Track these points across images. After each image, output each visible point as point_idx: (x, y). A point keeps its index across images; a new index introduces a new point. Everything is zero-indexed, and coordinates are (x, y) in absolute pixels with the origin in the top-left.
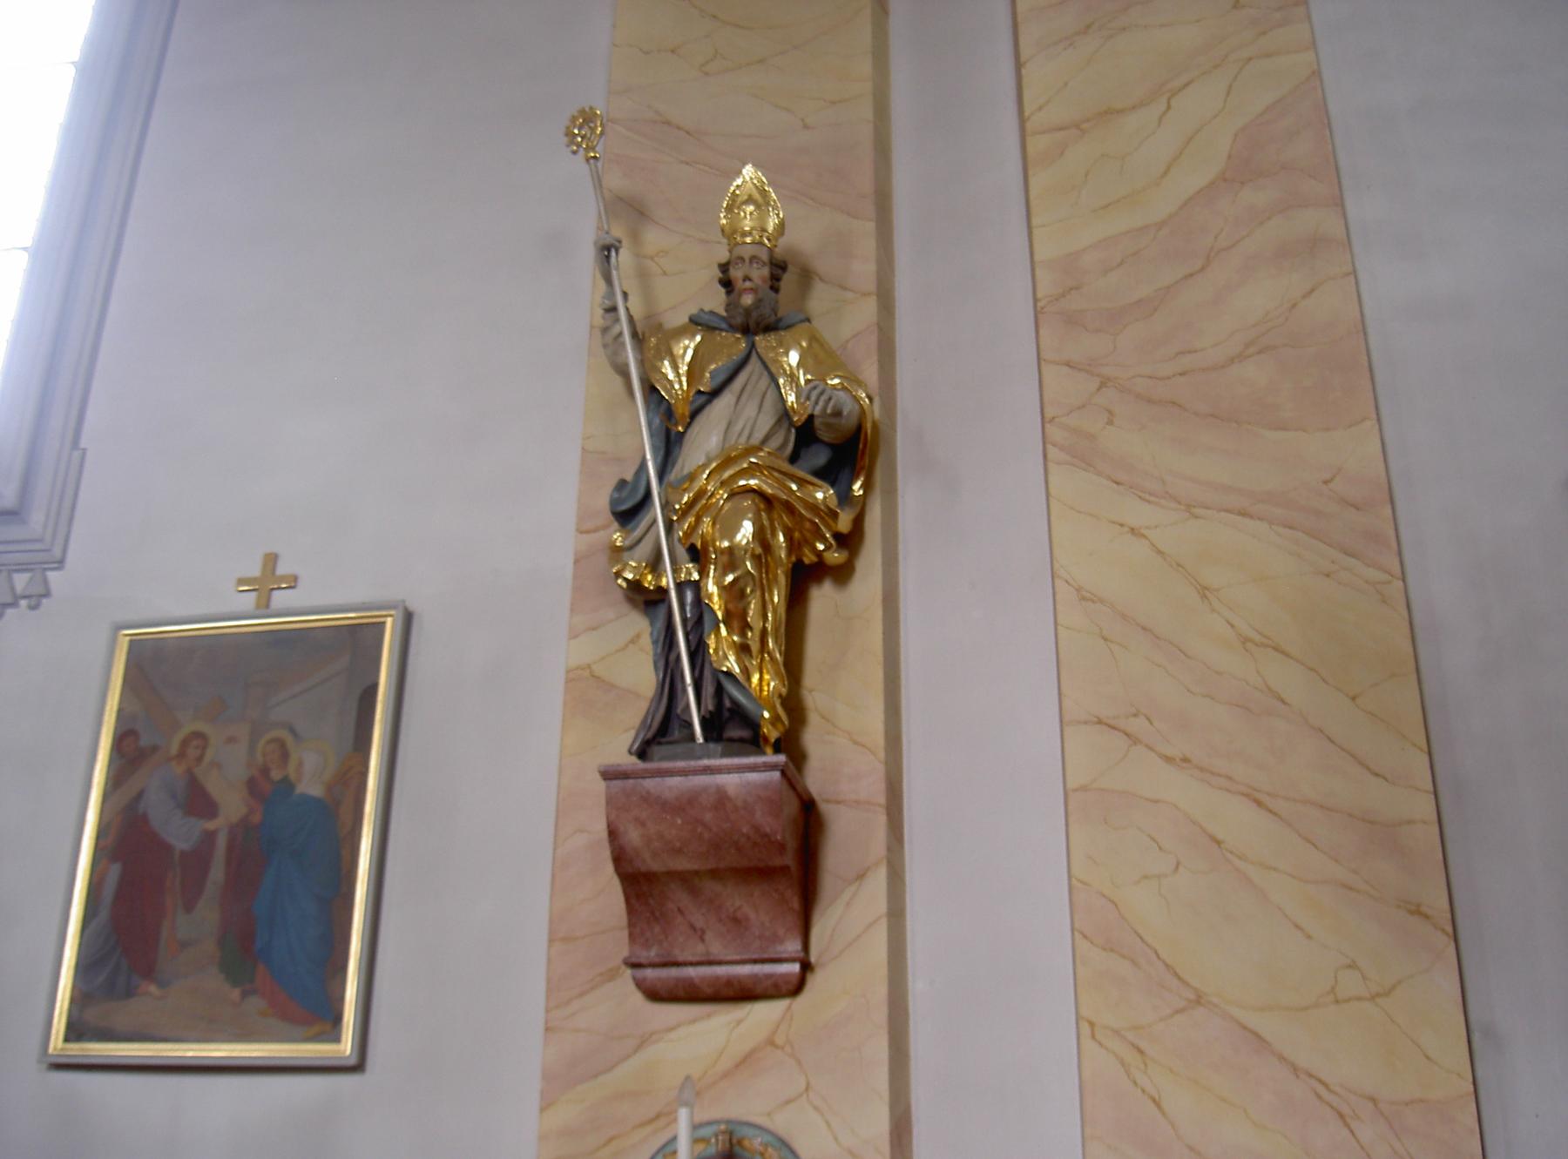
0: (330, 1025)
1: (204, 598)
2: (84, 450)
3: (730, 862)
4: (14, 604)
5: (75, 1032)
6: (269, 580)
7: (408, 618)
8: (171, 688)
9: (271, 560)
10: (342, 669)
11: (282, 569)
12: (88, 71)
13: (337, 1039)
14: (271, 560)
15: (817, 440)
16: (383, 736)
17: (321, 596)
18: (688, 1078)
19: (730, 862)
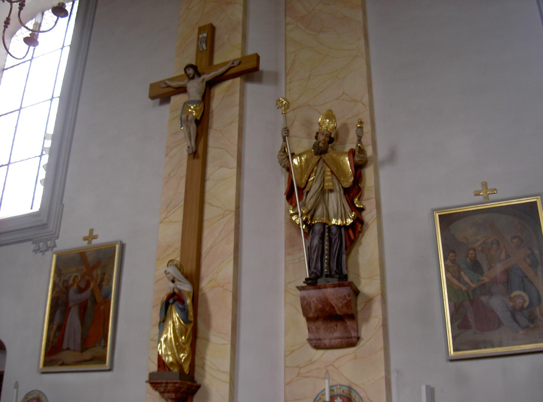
2: (63, 206)
3: (334, 310)
6: (91, 237)
7: (123, 247)
9: (91, 231)
11: (94, 234)
14: (91, 231)
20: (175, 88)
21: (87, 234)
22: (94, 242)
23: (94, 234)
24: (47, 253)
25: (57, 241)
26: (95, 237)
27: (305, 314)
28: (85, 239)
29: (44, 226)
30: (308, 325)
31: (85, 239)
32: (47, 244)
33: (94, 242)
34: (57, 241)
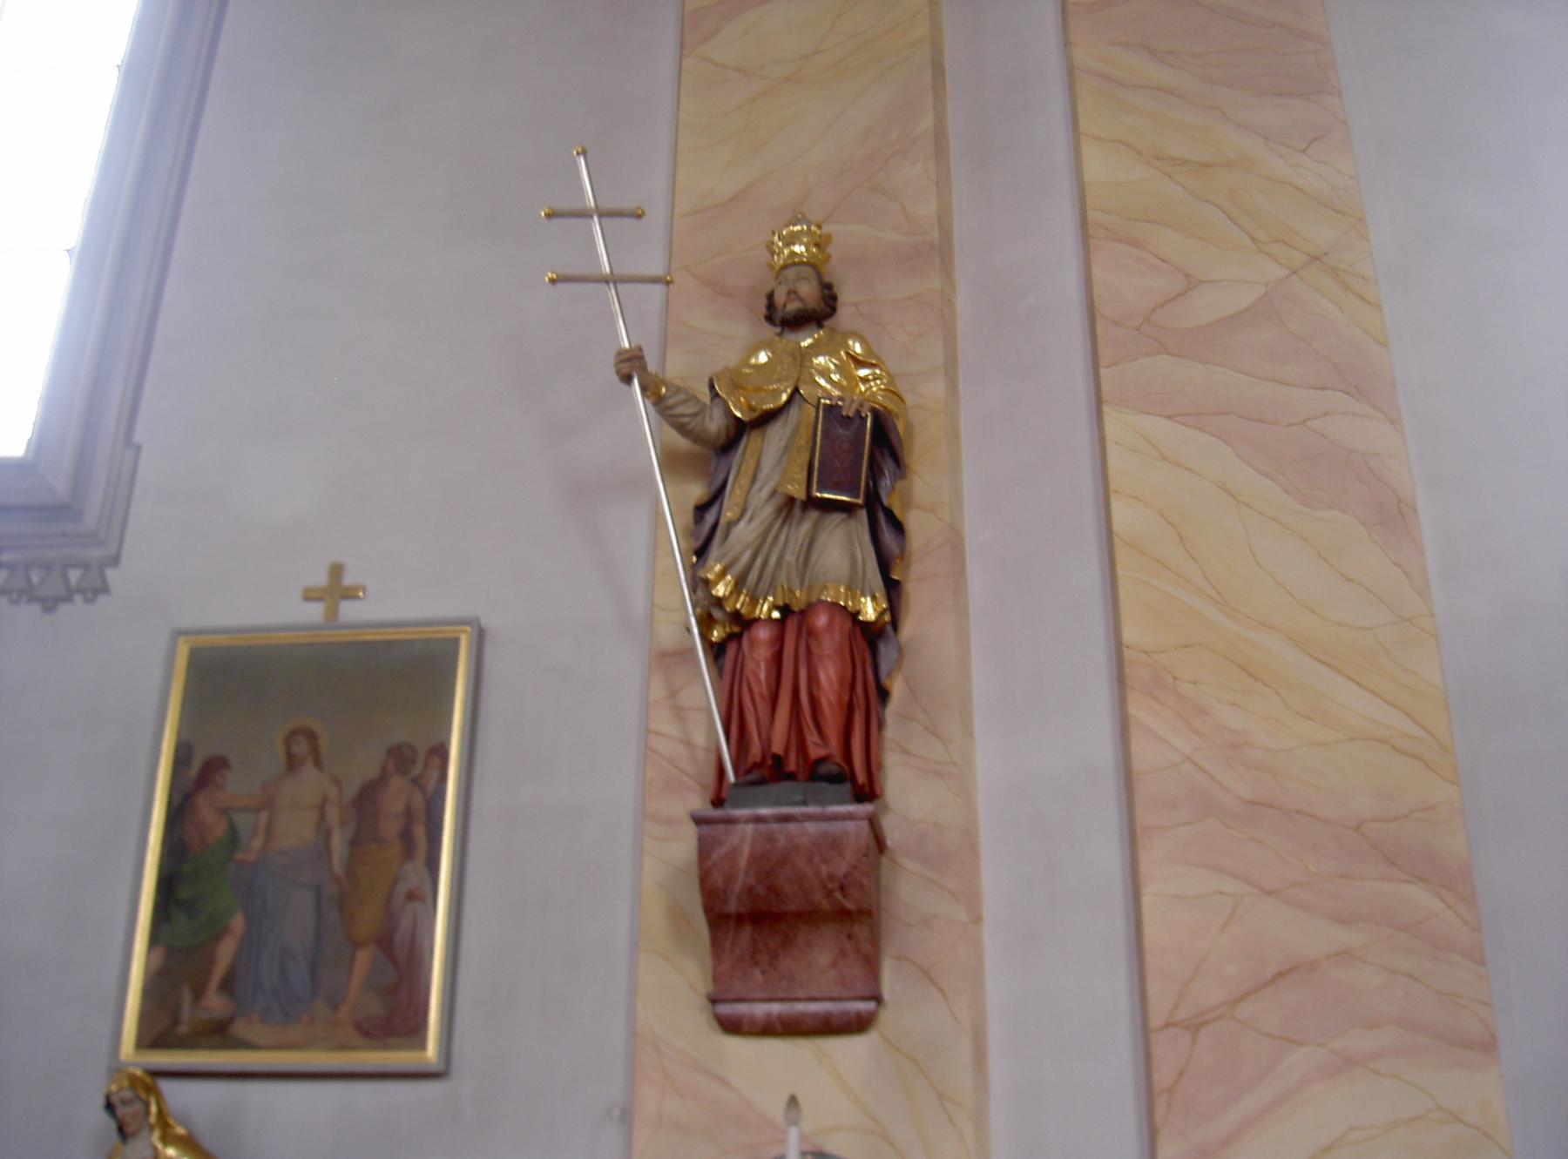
0: (414, 1031)
1: (267, 603)
2: (139, 448)
3: (791, 914)
4: (68, 599)
5: (151, 1038)
6: (337, 589)
7: (480, 637)
8: (228, 680)
9: (337, 571)
10: (411, 673)
11: (348, 580)
12: (132, 73)
13: (422, 1045)
14: (337, 571)
15: (793, 612)
16: (465, 703)
17: (391, 602)
18: (110, 1107)
19: (791, 914)
20: (1244, 801)
21: (321, 579)
22: (350, 611)
23: (348, 580)
24: (64, 608)
25: (110, 573)
26: (350, 594)
27: (708, 910)
28: (309, 596)
29: (59, 511)
30: (715, 968)
31: (309, 596)
32: (66, 580)
33: (350, 611)
34: (110, 573)
